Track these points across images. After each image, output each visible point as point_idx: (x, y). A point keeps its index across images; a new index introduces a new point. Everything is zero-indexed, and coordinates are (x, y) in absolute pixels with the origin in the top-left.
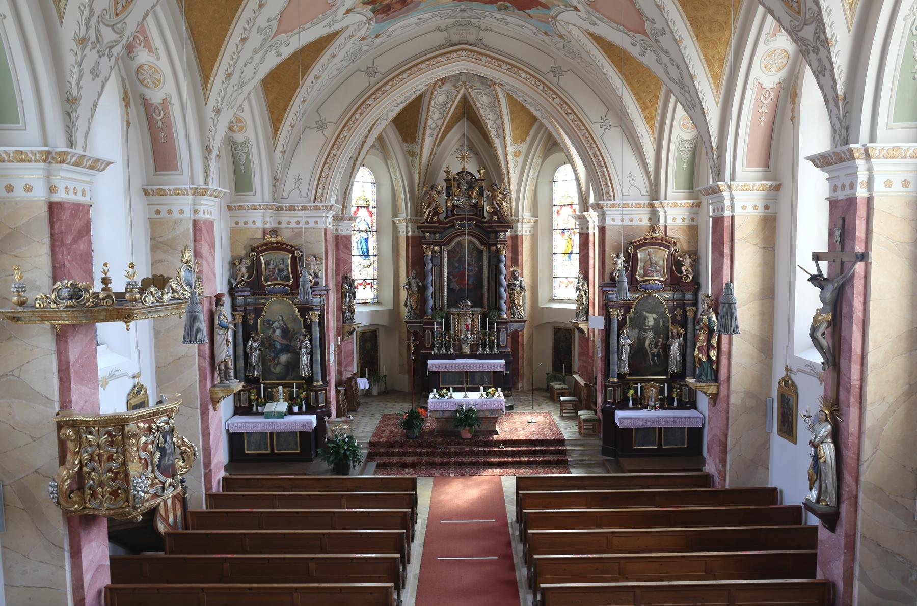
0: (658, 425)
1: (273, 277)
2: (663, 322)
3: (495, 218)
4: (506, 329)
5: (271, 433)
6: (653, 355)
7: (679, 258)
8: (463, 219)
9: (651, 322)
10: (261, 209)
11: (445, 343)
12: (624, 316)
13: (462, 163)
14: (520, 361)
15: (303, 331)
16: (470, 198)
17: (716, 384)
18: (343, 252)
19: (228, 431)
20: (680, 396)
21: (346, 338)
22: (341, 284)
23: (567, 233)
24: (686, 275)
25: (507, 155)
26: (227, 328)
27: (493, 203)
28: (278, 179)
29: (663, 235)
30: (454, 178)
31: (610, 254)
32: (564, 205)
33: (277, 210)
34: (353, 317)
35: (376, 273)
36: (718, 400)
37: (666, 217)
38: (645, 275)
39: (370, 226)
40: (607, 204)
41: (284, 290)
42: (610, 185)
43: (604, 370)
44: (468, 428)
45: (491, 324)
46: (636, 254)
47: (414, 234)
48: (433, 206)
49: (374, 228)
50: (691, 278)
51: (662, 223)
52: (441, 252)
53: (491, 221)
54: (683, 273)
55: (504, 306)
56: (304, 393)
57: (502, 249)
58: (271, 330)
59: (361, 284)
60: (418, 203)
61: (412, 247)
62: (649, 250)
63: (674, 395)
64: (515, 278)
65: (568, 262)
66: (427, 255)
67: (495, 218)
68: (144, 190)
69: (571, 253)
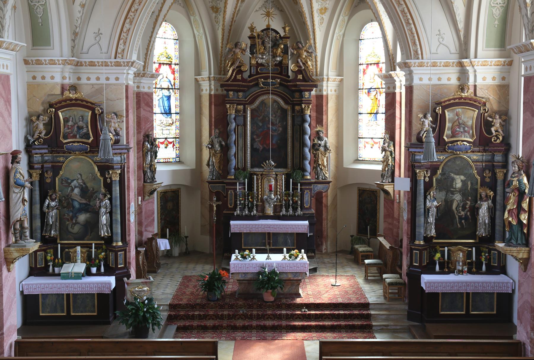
0: (466, 290)
1: (72, 135)
2: (472, 184)
3: (300, 77)
4: (310, 190)
5: (68, 295)
6: (461, 218)
7: (488, 118)
8: (266, 78)
9: (458, 184)
10: (59, 64)
11: (248, 204)
12: (431, 178)
13: (267, 20)
14: (324, 223)
15: (103, 190)
16: (274, 56)
17: (527, 249)
18: (144, 110)
19: (22, 292)
20: (488, 260)
21: (147, 198)
23: (373, 93)
24: (496, 136)
25: (312, 12)
26: (23, 186)
27: (298, 62)
28: (78, 33)
29: (473, 95)
30: (258, 35)
31: (417, 114)
32: (371, 64)
33: (77, 65)
35: (178, 131)
36: (529, 265)
37: (475, 76)
38: (453, 136)
39: (173, 84)
40: (415, 63)
42: (418, 43)
43: (409, 233)
44: (271, 291)
45: (295, 184)
46: (443, 115)
47: (217, 93)
48: (237, 64)
49: (176, 86)
50: (501, 139)
51: (471, 82)
52: (245, 111)
53: (296, 79)
54: (492, 134)
55: (308, 167)
56: (103, 254)
57: (306, 108)
58: (70, 189)
59: (162, 143)
60: (221, 61)
61: (215, 105)
62: (457, 110)
63: (483, 259)
64: (320, 139)
65: (372, 123)
66: (231, 114)
67: (300, 77)
69: (377, 113)
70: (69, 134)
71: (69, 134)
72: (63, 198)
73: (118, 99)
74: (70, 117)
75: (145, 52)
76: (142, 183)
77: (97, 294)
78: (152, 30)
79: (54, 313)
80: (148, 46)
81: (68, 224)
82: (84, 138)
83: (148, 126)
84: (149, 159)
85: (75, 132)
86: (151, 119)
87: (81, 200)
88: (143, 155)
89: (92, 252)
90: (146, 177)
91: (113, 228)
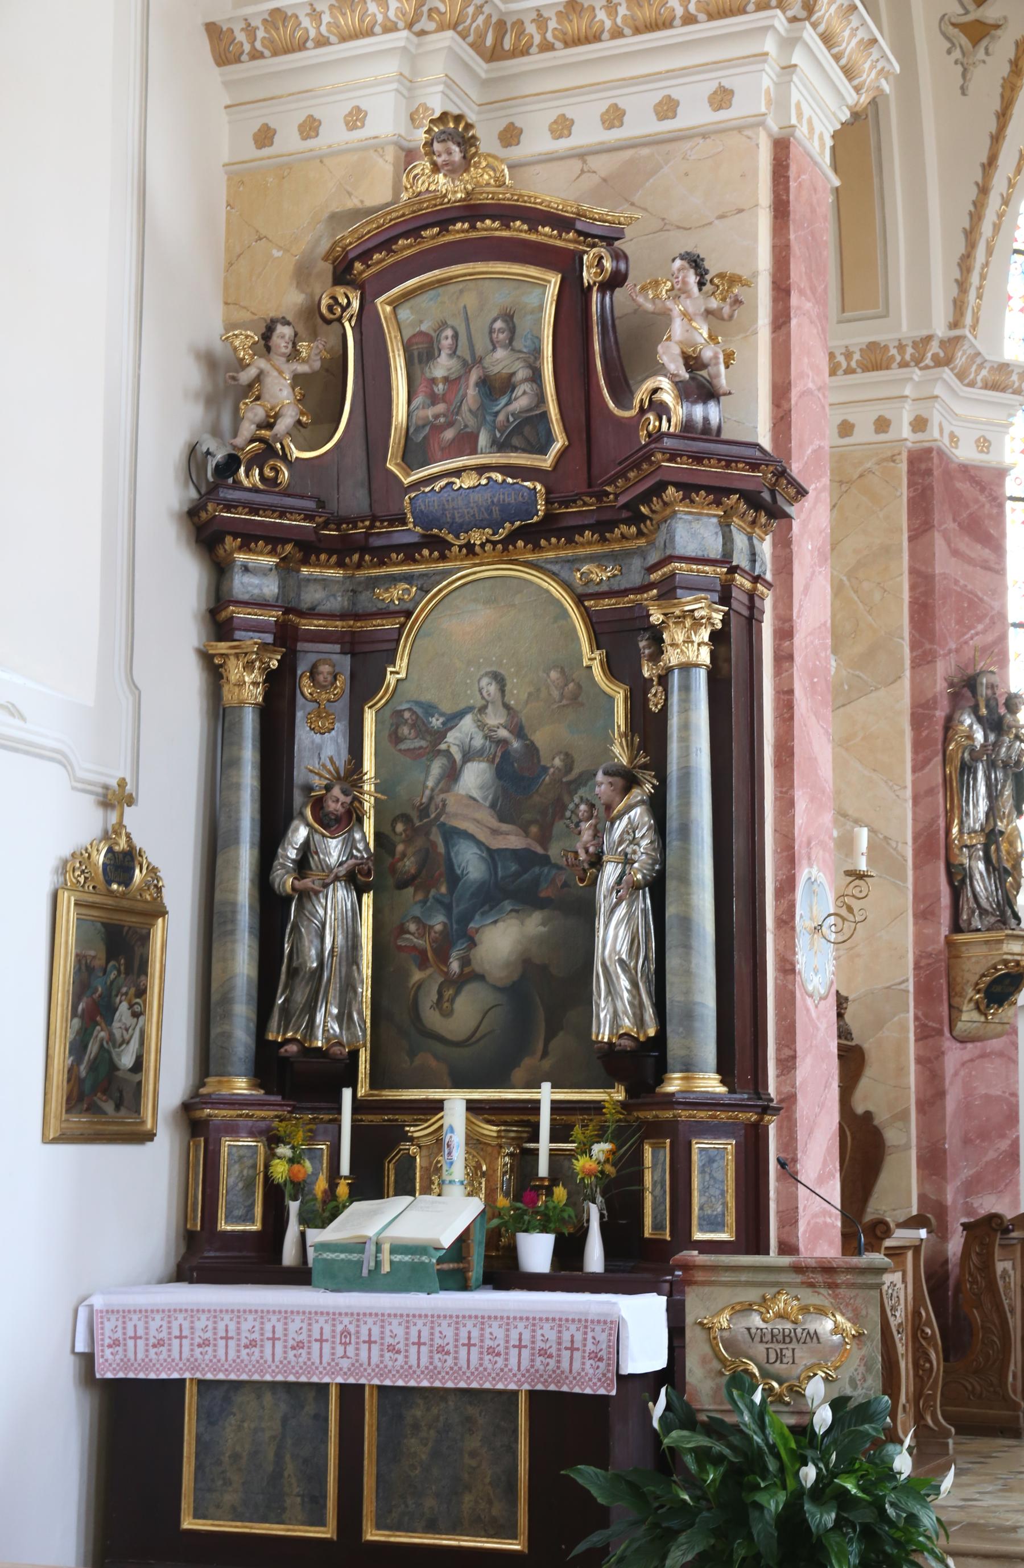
1: (449, 434)
5: (352, 1394)
15: (620, 754)
18: (955, 553)
19: (87, 1361)
21: (969, 1017)
22: (940, 714)
34: (1009, 900)
41: (510, 499)
56: (601, 1149)
58: (437, 768)
68: (213, 30)
70: (438, 429)
71: (438, 429)
72: (400, 827)
73: (722, 217)
74: (443, 325)
75: (961, 249)
76: (945, 930)
77: (532, 1394)
78: (993, 126)
79: (264, 1519)
80: (976, 216)
81: (420, 985)
82: (515, 449)
83: (978, 641)
84: (983, 806)
85: (466, 418)
86: (996, 605)
87: (495, 832)
88: (946, 781)
89: (535, 1153)
90: (967, 904)
91: (671, 979)
